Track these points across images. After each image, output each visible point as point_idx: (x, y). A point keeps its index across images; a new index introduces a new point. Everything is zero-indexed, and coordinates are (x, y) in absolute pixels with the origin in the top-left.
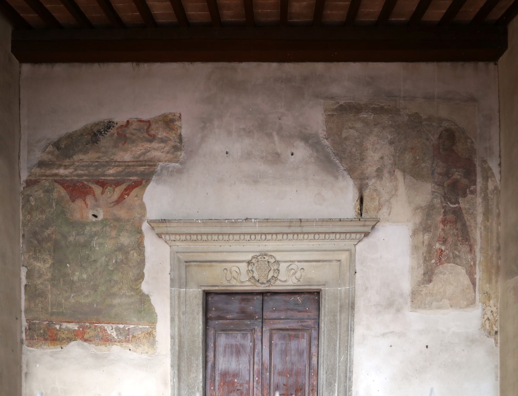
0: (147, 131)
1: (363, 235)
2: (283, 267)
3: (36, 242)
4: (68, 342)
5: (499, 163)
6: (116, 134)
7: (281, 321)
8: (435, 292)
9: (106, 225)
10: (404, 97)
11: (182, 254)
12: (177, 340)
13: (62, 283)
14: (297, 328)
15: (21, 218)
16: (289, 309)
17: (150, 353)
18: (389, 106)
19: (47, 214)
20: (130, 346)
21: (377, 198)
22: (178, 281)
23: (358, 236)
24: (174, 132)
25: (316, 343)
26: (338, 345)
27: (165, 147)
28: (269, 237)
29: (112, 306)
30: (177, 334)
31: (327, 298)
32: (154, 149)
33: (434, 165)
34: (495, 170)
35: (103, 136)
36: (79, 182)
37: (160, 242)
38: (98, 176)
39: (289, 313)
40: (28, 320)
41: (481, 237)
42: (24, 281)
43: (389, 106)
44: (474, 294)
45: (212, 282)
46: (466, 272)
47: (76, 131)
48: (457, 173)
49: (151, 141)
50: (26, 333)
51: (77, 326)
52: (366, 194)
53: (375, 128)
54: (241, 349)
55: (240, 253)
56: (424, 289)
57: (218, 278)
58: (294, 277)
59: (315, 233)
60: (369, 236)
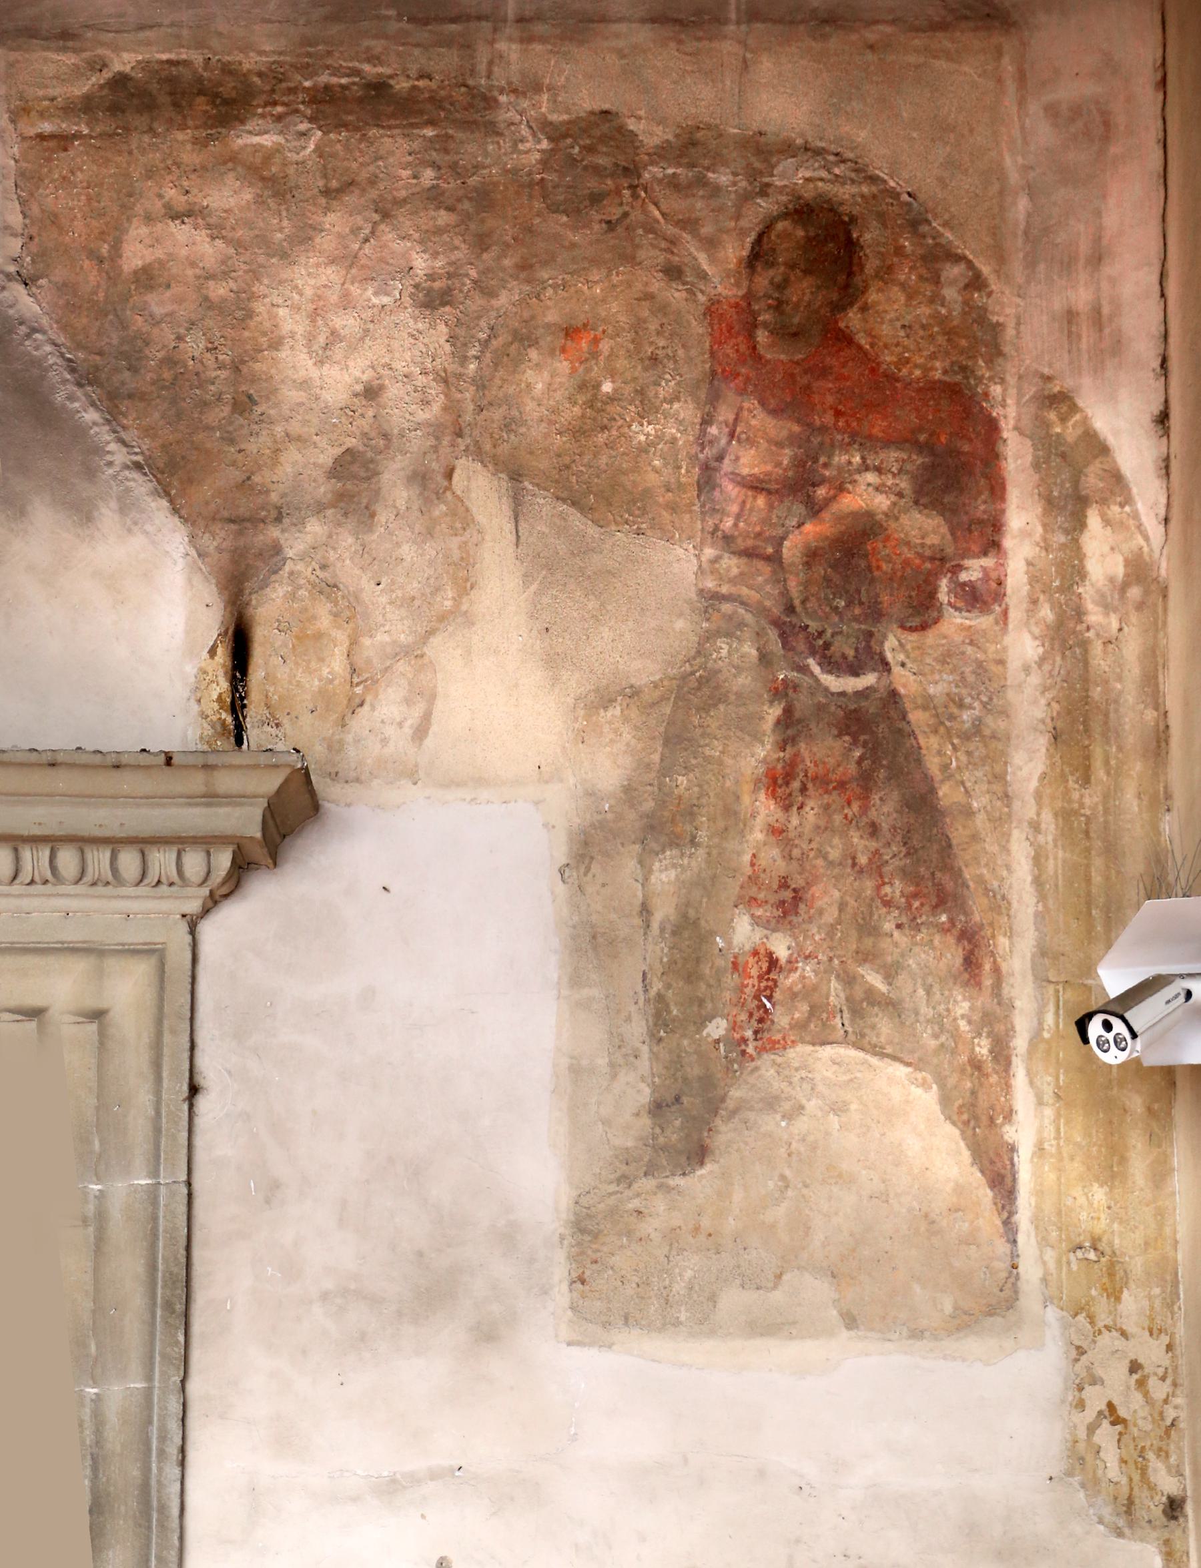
5: (1156, 408)
8: (731, 1224)
10: (520, 20)
18: (424, 75)
21: (341, 637)
33: (713, 430)
34: (1133, 449)
41: (1038, 882)
43: (424, 75)
44: (1002, 1248)
46: (945, 1101)
48: (871, 477)
52: (269, 609)
53: (327, 210)
56: (660, 1204)
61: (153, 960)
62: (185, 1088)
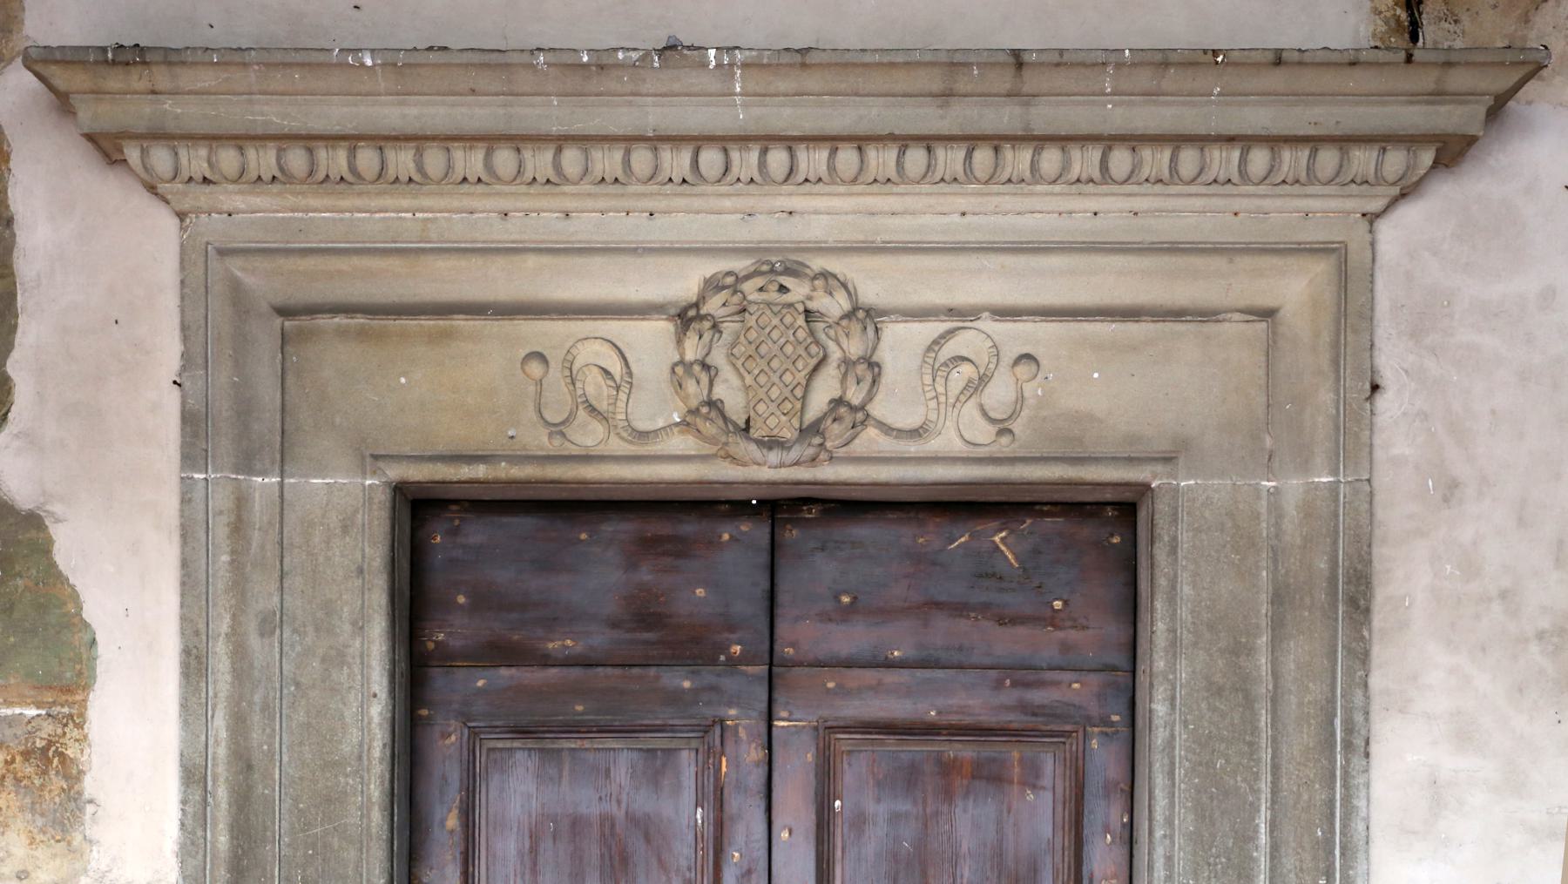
1: (1427, 157)
2: (901, 344)
7: (891, 677)
12: (222, 793)
14: (988, 719)
16: (938, 605)
22: (232, 429)
23: (1395, 161)
25: (1117, 815)
26: (1263, 838)
28: (813, 160)
30: (222, 751)
31: (1185, 537)
37: (114, 195)
39: (943, 632)
45: (452, 433)
54: (638, 847)
55: (630, 260)
57: (478, 409)
58: (970, 410)
59: (1109, 141)
60: (1466, 166)
61: (1333, 259)
62: (1368, 386)
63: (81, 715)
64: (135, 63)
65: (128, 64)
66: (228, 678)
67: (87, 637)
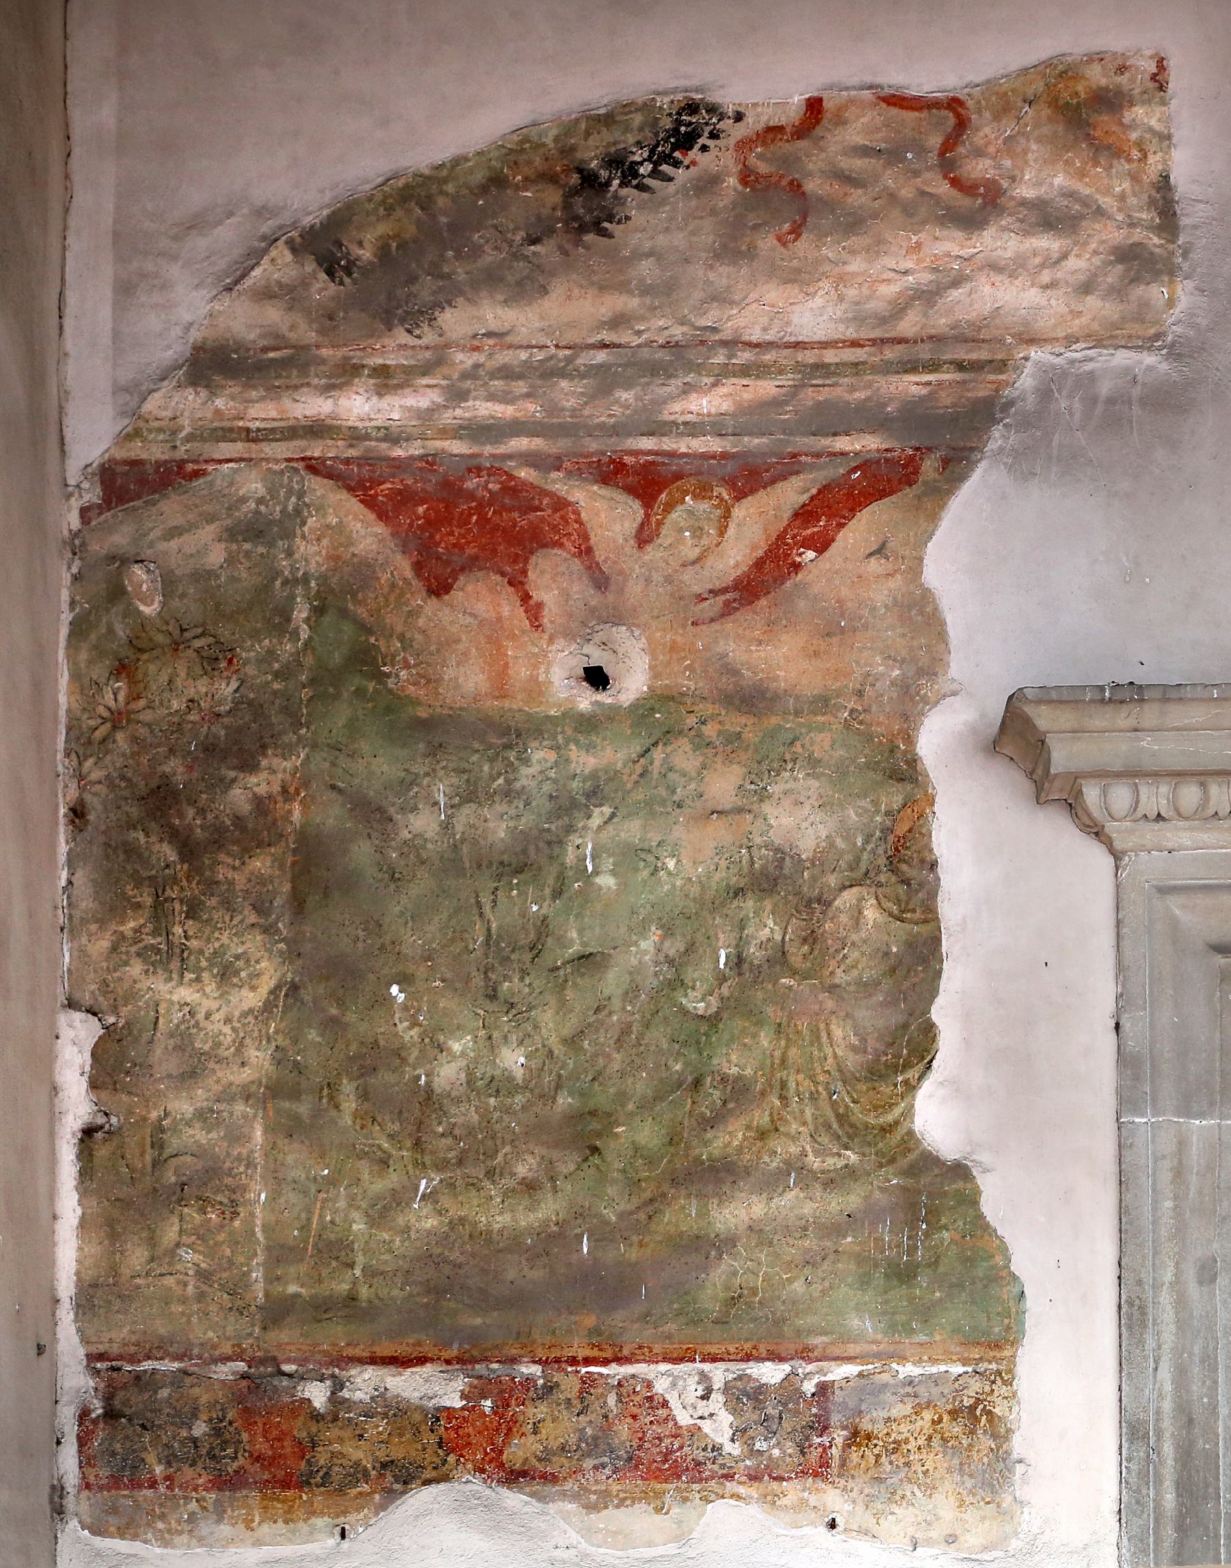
0: (947, 165)
3: (169, 853)
4: (391, 1496)
6: (732, 181)
9: (669, 734)
11: (1202, 900)
12: (1168, 1448)
13: (349, 1104)
15: (63, 699)
17: (972, 1540)
19: (250, 670)
20: (832, 1499)
24: (1122, 166)
27: (1064, 256)
29: (705, 1247)
30: (1167, 1405)
32: (994, 267)
35: (642, 188)
36: (478, 470)
38: (617, 430)
40: (101, 1357)
42: (77, 1105)
47: (457, 161)
49: (971, 222)
50: (82, 1441)
51: (460, 1383)
63: (1010, 1371)
64: (1132, 699)
65: (1122, 702)
66: (1173, 1328)
67: (1016, 1291)
